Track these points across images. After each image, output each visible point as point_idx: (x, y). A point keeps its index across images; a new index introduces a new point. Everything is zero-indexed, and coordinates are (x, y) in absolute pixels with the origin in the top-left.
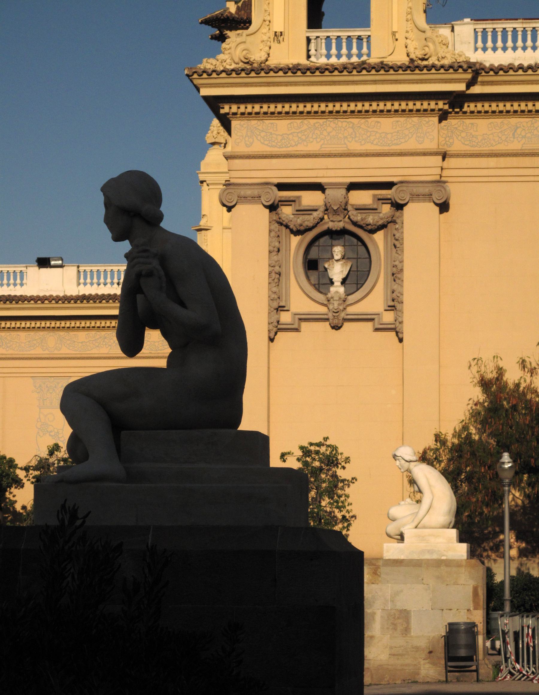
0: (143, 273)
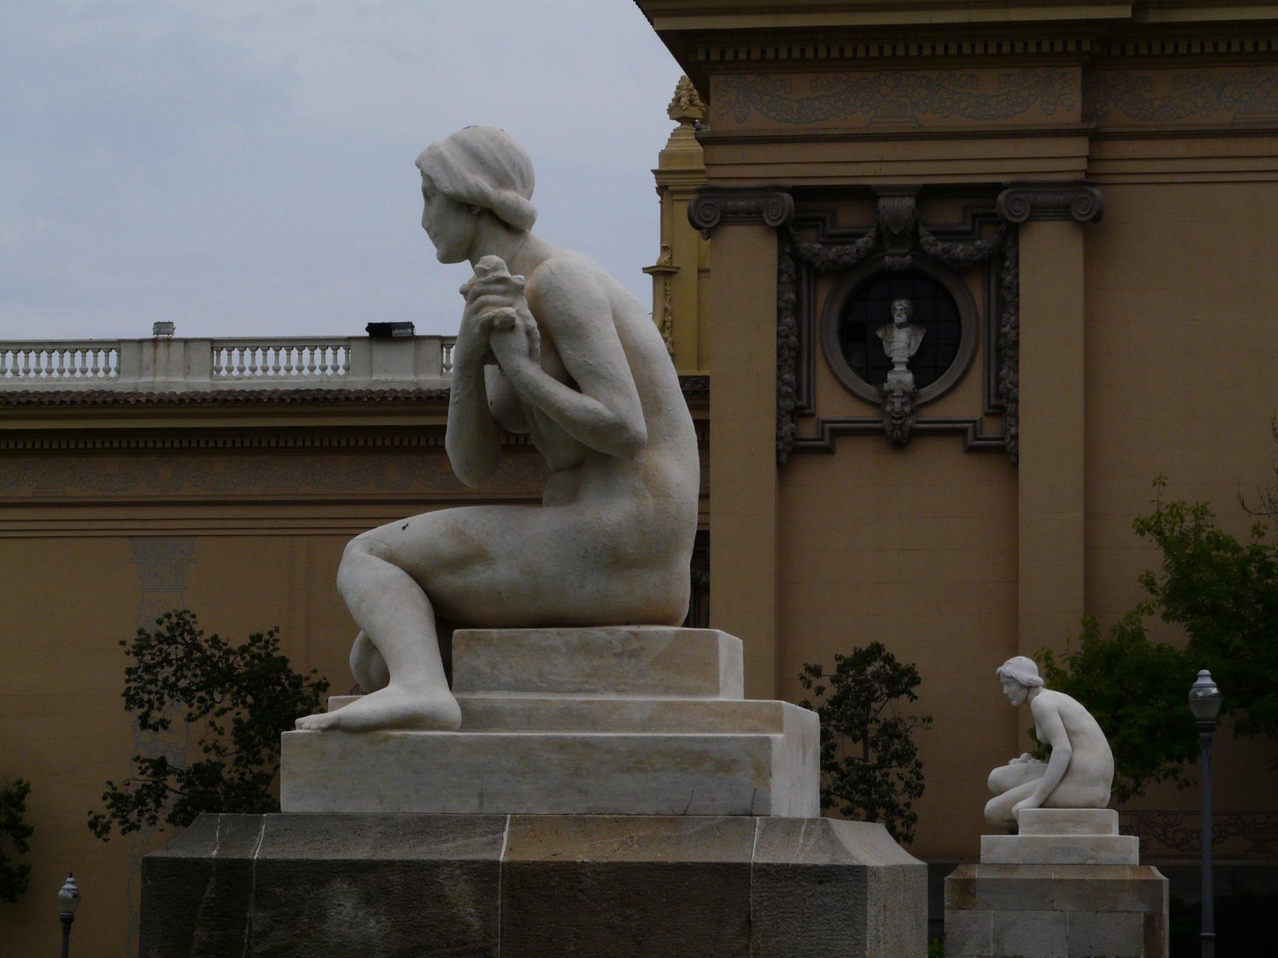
0: (496, 322)
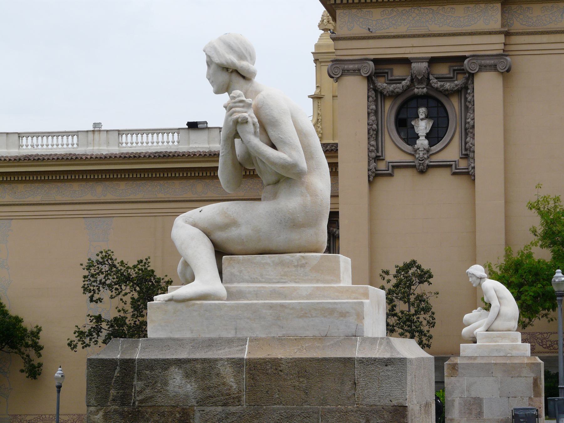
0: (240, 120)
